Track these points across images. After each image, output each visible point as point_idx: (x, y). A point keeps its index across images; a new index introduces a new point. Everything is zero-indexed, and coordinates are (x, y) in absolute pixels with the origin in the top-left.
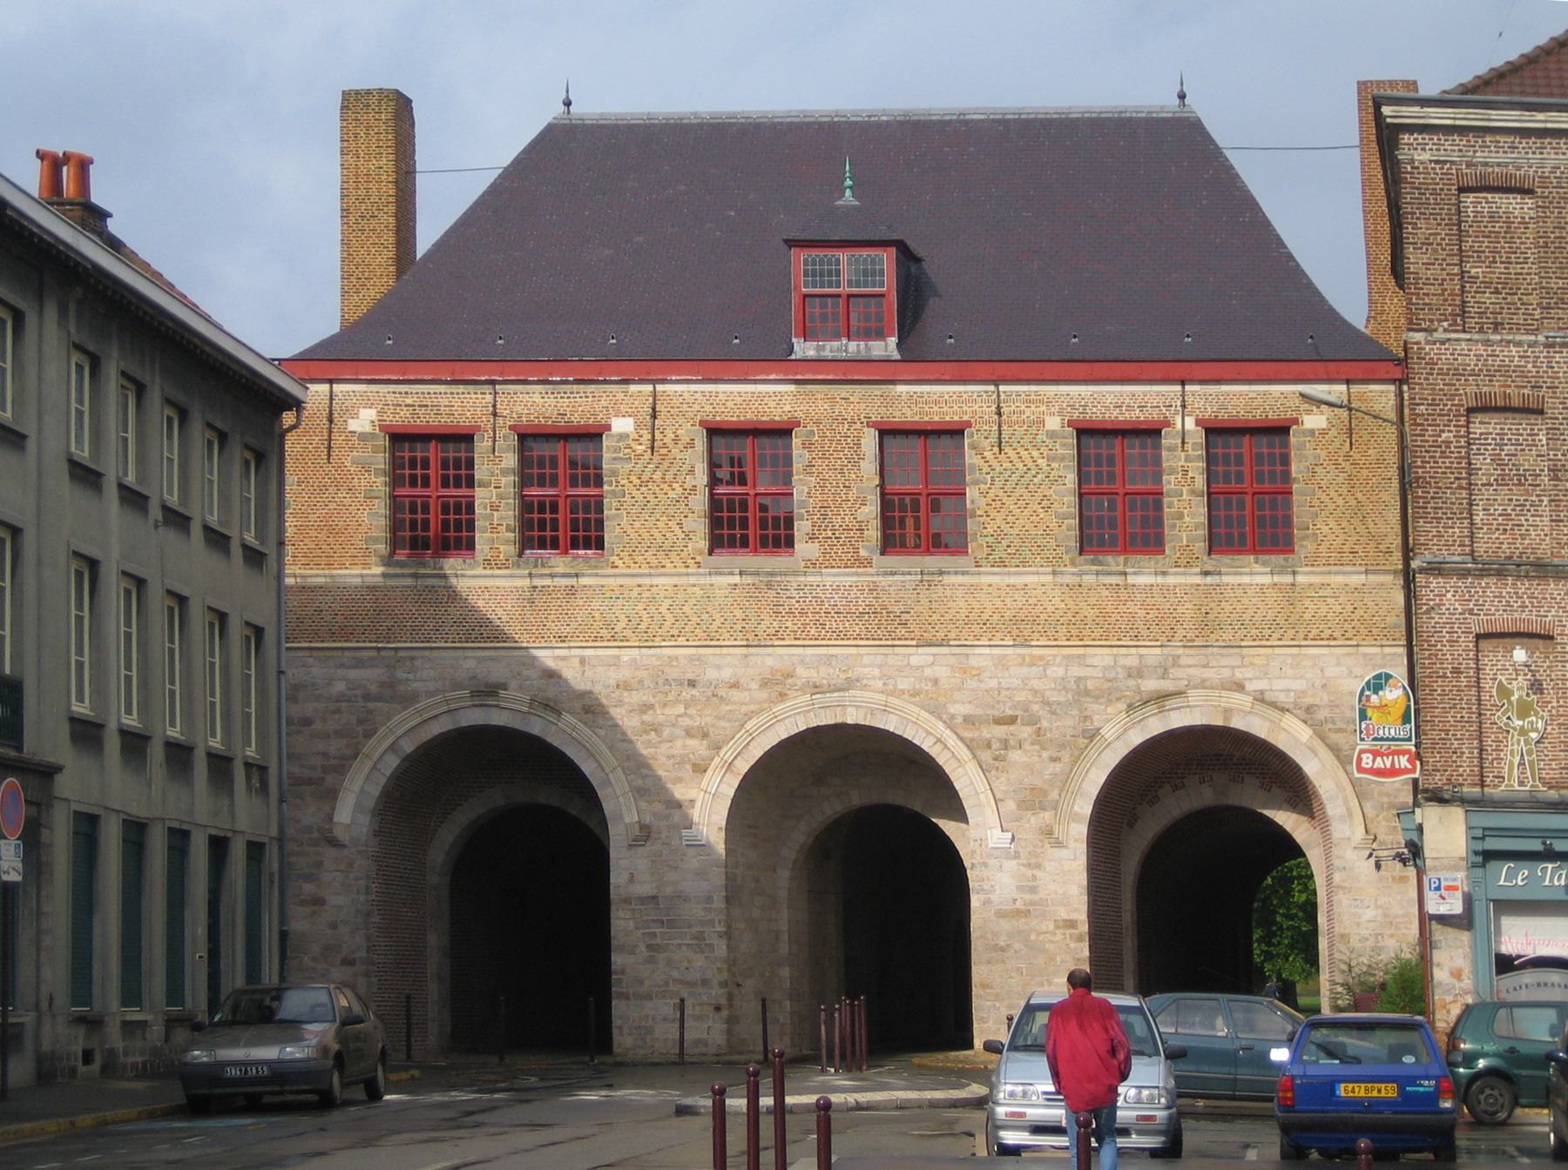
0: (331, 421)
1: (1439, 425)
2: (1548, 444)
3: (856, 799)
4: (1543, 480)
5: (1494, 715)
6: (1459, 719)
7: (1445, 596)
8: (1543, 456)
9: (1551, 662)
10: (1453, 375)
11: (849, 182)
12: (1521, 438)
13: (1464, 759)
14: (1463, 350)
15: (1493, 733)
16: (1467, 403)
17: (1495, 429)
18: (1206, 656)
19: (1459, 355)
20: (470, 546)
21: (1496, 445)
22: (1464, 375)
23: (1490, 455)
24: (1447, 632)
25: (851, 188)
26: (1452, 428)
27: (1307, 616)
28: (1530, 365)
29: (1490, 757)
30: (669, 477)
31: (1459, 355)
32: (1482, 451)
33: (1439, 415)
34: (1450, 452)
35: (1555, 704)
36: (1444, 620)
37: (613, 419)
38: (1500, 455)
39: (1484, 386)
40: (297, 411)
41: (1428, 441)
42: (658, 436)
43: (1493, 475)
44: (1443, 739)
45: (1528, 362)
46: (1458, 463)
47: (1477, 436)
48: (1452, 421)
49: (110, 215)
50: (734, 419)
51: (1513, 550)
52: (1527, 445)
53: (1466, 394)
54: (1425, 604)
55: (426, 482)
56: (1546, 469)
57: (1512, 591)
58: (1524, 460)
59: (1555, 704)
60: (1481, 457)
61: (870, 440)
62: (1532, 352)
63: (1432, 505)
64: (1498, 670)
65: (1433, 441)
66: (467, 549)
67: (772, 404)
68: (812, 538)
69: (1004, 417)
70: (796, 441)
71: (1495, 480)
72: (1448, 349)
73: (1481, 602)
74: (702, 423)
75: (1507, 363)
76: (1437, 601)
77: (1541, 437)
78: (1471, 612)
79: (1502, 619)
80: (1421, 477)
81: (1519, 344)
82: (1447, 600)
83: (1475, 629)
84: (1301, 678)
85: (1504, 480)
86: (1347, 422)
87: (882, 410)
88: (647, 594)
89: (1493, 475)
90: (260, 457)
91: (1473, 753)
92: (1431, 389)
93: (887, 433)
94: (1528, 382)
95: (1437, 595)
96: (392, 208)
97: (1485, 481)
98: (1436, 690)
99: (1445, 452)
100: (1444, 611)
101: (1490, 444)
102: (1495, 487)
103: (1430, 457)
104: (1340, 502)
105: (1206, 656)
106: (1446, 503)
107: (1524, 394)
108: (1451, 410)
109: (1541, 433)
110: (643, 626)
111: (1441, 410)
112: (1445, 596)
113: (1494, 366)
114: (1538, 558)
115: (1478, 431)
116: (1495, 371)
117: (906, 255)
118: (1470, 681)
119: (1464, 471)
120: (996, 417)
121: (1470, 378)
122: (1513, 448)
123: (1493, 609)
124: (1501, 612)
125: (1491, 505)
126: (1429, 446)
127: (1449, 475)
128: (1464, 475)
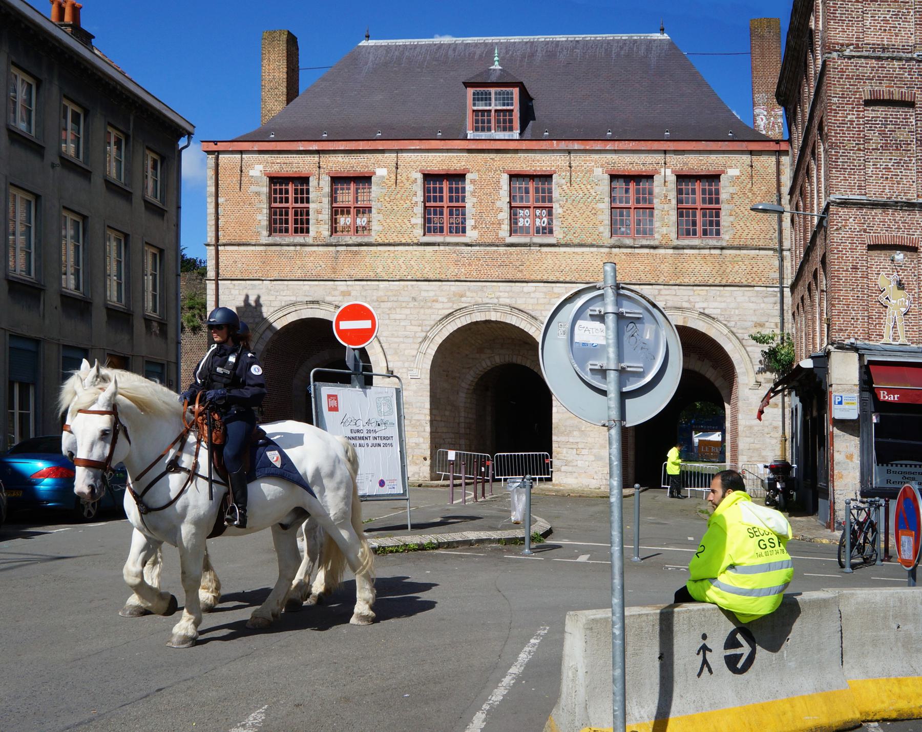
0: (241, 171)
1: (846, 110)
2: (917, 124)
3: (498, 360)
4: (913, 148)
5: (878, 296)
6: (856, 298)
7: (848, 220)
8: (913, 132)
9: (915, 264)
10: (856, 79)
11: (496, 58)
12: (898, 120)
13: (859, 323)
14: (863, 63)
15: (876, 307)
16: (865, 97)
17: (882, 114)
18: (675, 290)
19: (860, 66)
20: (308, 231)
21: (882, 124)
22: (863, 79)
23: (878, 131)
24: (849, 243)
25: (498, 61)
26: (855, 113)
27: (728, 271)
28: (906, 74)
29: (874, 323)
30: (404, 196)
31: (860, 66)
32: (873, 128)
33: (846, 104)
34: (853, 128)
35: (917, 291)
36: (848, 236)
37: (377, 169)
38: (884, 131)
39: (877, 86)
40: (188, 138)
41: (838, 120)
42: (399, 177)
43: (879, 143)
44: (846, 310)
45: (905, 72)
46: (858, 134)
47: (870, 119)
48: (854, 108)
49: (94, 37)
50: (437, 169)
51: (892, 193)
52: (902, 125)
53: (864, 91)
54: (836, 225)
55: (287, 201)
56: (915, 140)
57: (892, 218)
58: (900, 134)
59: (917, 291)
60: (872, 132)
61: (505, 178)
62: (908, 65)
63: (841, 160)
64: (880, 268)
65: (842, 120)
66: (306, 233)
67: (455, 161)
68: (475, 228)
69: (573, 168)
70: (467, 181)
71: (881, 146)
72: (853, 63)
73: (871, 225)
74: (421, 171)
75: (891, 72)
76: (843, 224)
77: (911, 120)
78: (865, 231)
79: (885, 237)
80: (834, 143)
81: (900, 59)
82: (850, 223)
83: (868, 242)
84: (724, 302)
85: (887, 147)
86: (750, 173)
87: (511, 165)
88: (392, 255)
89: (879, 143)
90: (163, 159)
91: (864, 319)
92: (841, 88)
93: (513, 177)
94: (905, 84)
95: (844, 220)
96: (285, 84)
97: (874, 147)
98: (842, 279)
99: (850, 127)
100: (847, 230)
101: (878, 124)
102: (881, 151)
103: (840, 130)
104: (746, 213)
105: (675, 290)
106: (850, 159)
107: (902, 92)
108: (854, 101)
109: (912, 117)
110: (391, 270)
111: (847, 101)
112: (848, 220)
113: (883, 74)
114: (908, 199)
115: (871, 115)
116: (883, 77)
117: (520, 85)
118: (864, 274)
119: (862, 139)
120: (569, 168)
121: (867, 81)
122: (893, 126)
123: (879, 229)
124: (884, 231)
125: (878, 162)
126: (839, 123)
127: (852, 142)
128: (862, 142)
